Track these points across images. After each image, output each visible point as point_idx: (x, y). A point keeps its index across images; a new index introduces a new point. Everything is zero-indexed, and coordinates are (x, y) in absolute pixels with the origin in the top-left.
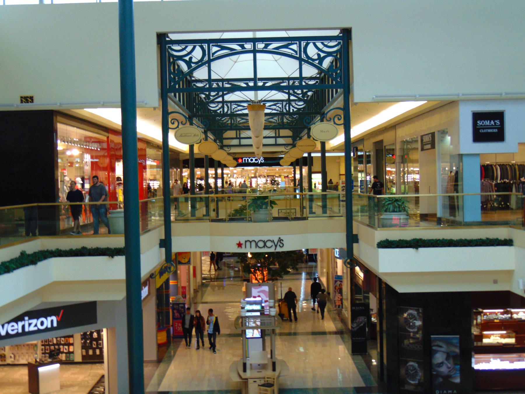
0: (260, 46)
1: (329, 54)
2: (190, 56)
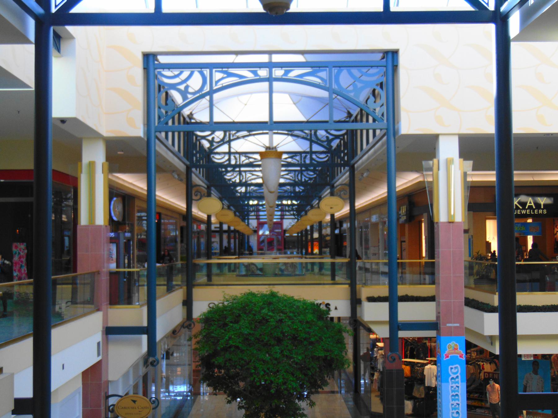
0: (278, 73)
1: (337, 137)
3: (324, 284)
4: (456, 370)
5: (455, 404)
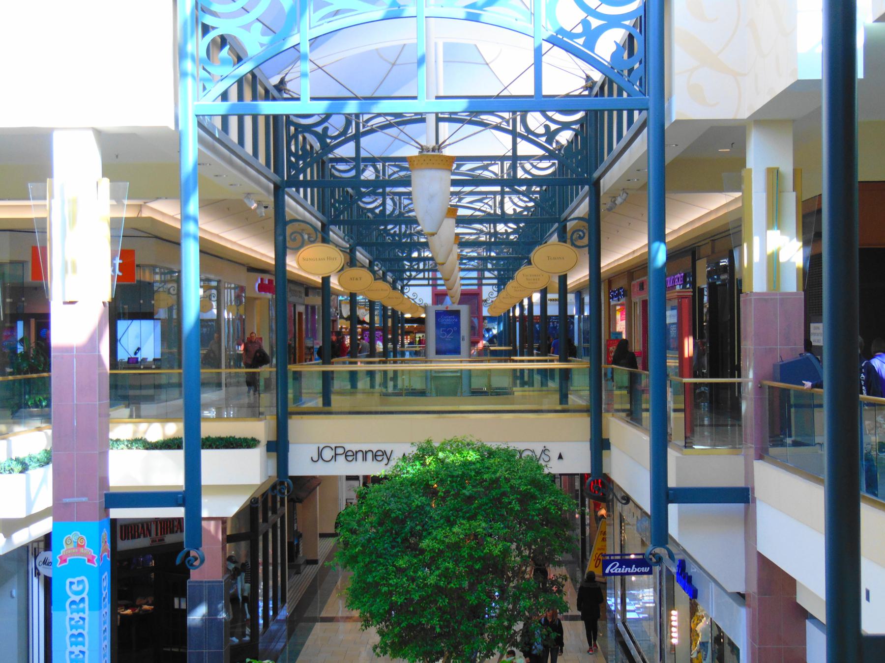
2: (326, 125)
3: (376, 413)
4: (81, 587)
5: (77, 652)
